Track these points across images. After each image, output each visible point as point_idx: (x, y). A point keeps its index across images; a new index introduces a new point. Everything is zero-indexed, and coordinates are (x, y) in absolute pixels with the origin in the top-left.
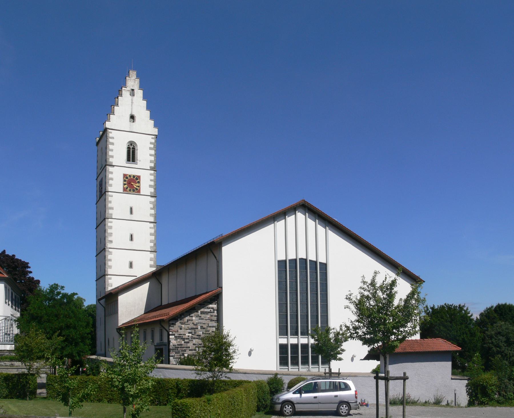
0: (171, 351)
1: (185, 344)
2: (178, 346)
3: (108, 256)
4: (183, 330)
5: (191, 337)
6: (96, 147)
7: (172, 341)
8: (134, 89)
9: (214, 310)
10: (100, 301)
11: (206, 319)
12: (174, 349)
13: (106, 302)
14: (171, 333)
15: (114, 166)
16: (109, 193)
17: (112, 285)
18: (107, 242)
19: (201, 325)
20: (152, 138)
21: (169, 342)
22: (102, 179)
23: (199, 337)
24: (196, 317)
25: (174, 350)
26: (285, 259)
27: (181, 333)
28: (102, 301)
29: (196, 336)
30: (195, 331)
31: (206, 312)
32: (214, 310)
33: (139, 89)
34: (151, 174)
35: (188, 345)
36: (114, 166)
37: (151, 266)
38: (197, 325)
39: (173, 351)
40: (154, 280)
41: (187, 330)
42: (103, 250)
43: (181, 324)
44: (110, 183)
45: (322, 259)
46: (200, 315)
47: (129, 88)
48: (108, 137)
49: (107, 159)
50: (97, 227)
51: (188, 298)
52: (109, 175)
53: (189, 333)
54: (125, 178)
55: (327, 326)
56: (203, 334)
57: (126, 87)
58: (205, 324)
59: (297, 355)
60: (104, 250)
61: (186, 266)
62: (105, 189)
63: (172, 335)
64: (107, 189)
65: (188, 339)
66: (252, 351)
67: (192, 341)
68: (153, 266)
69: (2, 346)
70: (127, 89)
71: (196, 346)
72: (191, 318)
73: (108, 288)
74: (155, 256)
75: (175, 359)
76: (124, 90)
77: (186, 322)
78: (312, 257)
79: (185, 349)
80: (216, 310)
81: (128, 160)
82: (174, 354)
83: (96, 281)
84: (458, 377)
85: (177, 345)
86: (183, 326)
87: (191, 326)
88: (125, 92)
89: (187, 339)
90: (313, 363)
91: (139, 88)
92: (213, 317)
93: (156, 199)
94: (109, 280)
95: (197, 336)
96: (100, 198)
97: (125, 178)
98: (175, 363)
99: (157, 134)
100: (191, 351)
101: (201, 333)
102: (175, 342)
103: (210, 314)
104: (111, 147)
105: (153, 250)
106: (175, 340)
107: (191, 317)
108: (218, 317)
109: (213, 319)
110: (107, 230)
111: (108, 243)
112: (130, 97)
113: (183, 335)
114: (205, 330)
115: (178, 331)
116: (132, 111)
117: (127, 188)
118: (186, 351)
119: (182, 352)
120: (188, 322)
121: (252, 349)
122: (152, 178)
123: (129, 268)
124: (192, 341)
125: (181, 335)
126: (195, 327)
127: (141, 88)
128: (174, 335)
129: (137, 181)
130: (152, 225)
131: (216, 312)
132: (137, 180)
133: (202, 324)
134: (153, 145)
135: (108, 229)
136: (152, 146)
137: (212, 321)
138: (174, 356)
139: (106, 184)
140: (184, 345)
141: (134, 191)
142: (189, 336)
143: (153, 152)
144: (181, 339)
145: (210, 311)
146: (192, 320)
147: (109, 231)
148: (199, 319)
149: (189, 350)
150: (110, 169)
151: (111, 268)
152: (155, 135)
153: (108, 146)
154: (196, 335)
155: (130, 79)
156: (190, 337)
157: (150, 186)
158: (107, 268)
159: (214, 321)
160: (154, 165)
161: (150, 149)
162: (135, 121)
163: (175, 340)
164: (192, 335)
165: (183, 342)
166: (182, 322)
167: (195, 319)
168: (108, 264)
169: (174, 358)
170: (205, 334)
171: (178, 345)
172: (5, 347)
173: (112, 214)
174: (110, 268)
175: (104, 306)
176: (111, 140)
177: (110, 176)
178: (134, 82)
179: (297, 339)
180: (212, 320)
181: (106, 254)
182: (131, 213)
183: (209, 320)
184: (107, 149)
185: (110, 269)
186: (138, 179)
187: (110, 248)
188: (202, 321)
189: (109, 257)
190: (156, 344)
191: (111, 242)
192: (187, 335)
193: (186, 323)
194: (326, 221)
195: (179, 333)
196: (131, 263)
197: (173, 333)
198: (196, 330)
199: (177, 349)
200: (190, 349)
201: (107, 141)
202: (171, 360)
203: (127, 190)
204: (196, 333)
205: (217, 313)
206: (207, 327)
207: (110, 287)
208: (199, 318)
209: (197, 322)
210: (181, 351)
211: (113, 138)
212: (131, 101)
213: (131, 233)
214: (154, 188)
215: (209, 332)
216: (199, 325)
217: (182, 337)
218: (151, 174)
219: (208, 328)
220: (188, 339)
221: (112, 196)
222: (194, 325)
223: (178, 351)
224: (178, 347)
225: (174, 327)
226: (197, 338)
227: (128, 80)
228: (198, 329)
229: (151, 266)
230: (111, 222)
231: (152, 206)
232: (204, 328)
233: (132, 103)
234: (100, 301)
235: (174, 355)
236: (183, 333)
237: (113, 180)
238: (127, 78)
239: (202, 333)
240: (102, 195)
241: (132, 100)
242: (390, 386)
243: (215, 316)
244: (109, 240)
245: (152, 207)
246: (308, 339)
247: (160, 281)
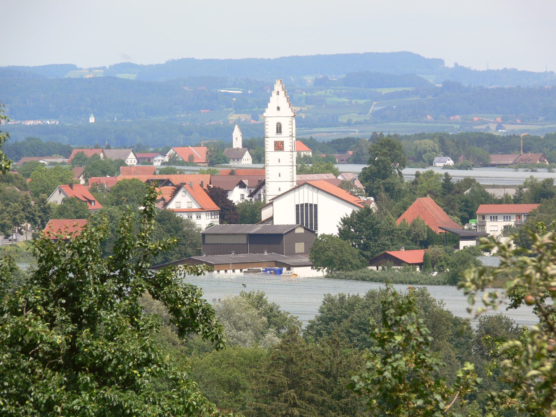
81: (277, 132)
88: (274, 94)
150: (266, 139)
182: (279, 162)
211: (268, 122)
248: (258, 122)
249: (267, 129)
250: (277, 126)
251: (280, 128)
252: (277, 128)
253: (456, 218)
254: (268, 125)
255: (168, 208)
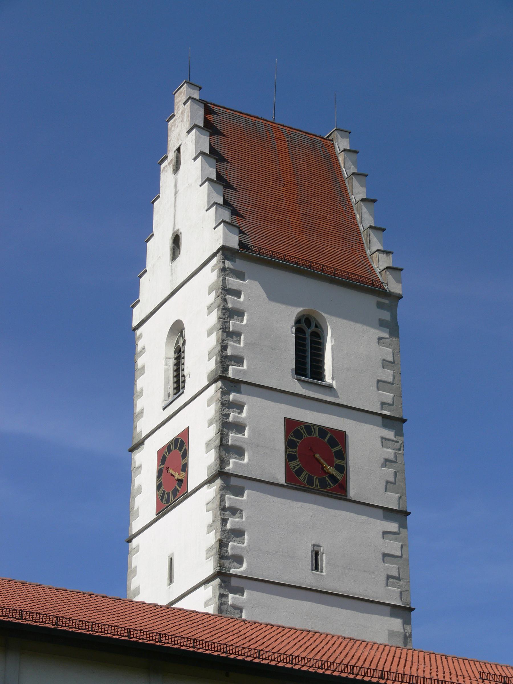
10: (399, 532)
54: (291, 433)
55: (239, 340)
84: (302, 335)
97: (291, 433)
117: (299, 472)
129: (334, 450)
132: (325, 438)
182: (316, 566)
186: (338, 445)
203: (302, 478)
234: (399, 532)
242: (350, 476)
246: (233, 476)
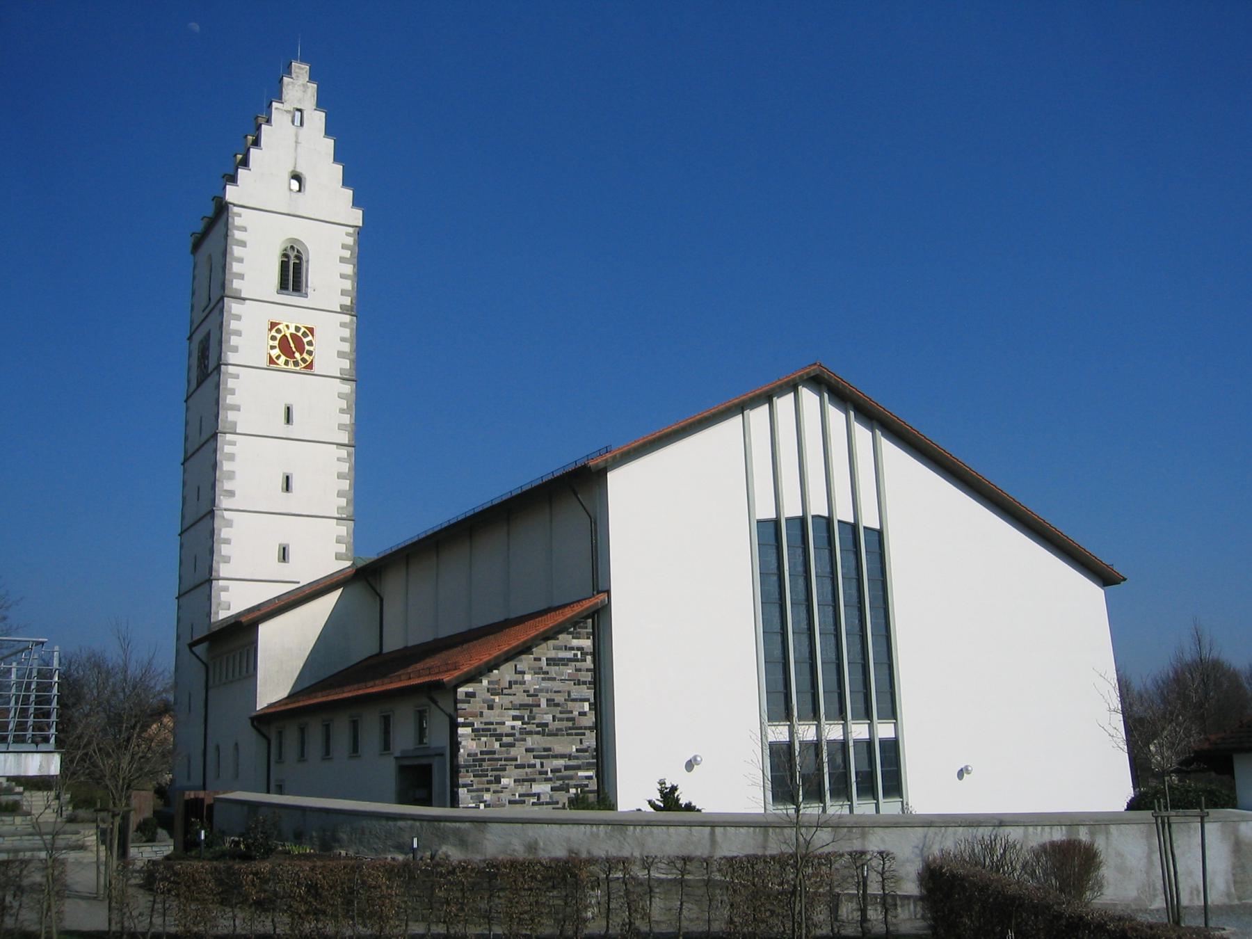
0: (462, 770)
1: (503, 749)
2: (485, 756)
3: (220, 530)
4: (496, 711)
5: (520, 729)
6: (192, 256)
7: (464, 743)
8: (303, 108)
9: (584, 654)
10: (194, 649)
11: (563, 678)
12: (469, 766)
13: (209, 650)
14: (461, 720)
15: (244, 299)
16: (230, 367)
17: (230, 606)
18: (220, 495)
19: (549, 696)
20: (348, 234)
21: (455, 745)
22: (209, 334)
23: (544, 730)
24: (535, 673)
25: (470, 767)
26: (774, 517)
27: (492, 720)
28: (200, 649)
29: (535, 726)
30: (531, 712)
31: (563, 659)
32: (584, 654)
33: (315, 110)
34: (343, 325)
35: (512, 753)
36: (244, 299)
37: (339, 557)
38: (537, 695)
39: (467, 771)
40: (358, 589)
41: (509, 711)
42: (205, 516)
43: (491, 695)
44: (232, 343)
45: (869, 520)
46: (545, 668)
47: (288, 106)
48: (230, 226)
49: (226, 282)
50: (186, 460)
51: (443, 639)
52: (232, 321)
53: (515, 718)
56: (554, 720)
57: (282, 103)
58: (559, 692)
59: (895, 768)
60: (209, 517)
61: (438, 556)
62: (220, 358)
63: (465, 725)
64: (223, 358)
65: (512, 735)
66: (698, 764)
67: (524, 740)
68: (344, 557)
69: (5, 761)
70: (285, 108)
71: (534, 753)
72: (521, 676)
73: (217, 613)
74: (351, 531)
75: (474, 794)
76: (276, 108)
77: (506, 688)
78: (844, 513)
79: (503, 763)
80: (591, 654)
81: (283, 286)
82: (472, 779)
83: (176, 598)
85: (479, 754)
86: (497, 699)
87: (522, 698)
88: (279, 113)
89: (508, 735)
90: (860, 793)
91: (315, 107)
92: (582, 673)
93: (354, 387)
94: (222, 593)
95: (537, 727)
96: (199, 385)
98: (474, 805)
99: (361, 225)
100: (520, 770)
101: (548, 718)
102: (475, 746)
103: (573, 664)
104: (237, 251)
105: (344, 516)
106: (472, 740)
107: (518, 675)
108: (595, 674)
109: (582, 679)
110: (221, 462)
111: (222, 497)
112: (292, 129)
113: (497, 723)
114: (560, 708)
115: (482, 713)
116: (296, 164)
118: (505, 770)
119: (494, 772)
120: (510, 687)
121: (699, 759)
122: (347, 333)
123: (279, 561)
124: (524, 740)
125: (492, 724)
126: (530, 700)
127: (320, 105)
128: (472, 725)
130: (343, 453)
131: (589, 658)
133: (551, 692)
134: (350, 252)
135: (224, 462)
136: (347, 254)
137: (579, 684)
138: (472, 785)
139: (221, 346)
140: (501, 753)
141: (298, 366)
142: (513, 728)
143: (349, 269)
144: (491, 735)
145: (572, 656)
146: (523, 683)
147: (226, 466)
148: (543, 679)
149: (513, 767)
150: (233, 307)
151: (229, 562)
152: (356, 227)
153: (231, 248)
154: (533, 724)
155: (292, 83)
156: (517, 729)
157: (341, 354)
158: (218, 563)
159: (584, 683)
160: (351, 302)
161: (342, 260)
162: (302, 188)
163: (475, 740)
164: (523, 724)
165: (497, 745)
166: (495, 689)
167: (530, 679)
168: (221, 552)
169: (468, 791)
170: (561, 720)
171: (482, 753)
172: (19, 764)
173: (235, 424)
174: (225, 562)
175: (204, 659)
176: (238, 235)
177: (234, 325)
178: (304, 92)
179: (893, 725)
180: (579, 680)
181: (215, 526)
182: (288, 420)
183: (573, 683)
184: (228, 256)
185: (226, 564)
186: (308, 336)
187: (225, 510)
188: (550, 685)
189: (224, 533)
190: (397, 754)
191: (231, 494)
192: (509, 723)
193: (505, 691)
194: (875, 422)
195: (484, 720)
196: (284, 549)
197: (467, 721)
198: (534, 709)
199: (480, 766)
200: (519, 762)
201: (227, 236)
202: (460, 795)
204: (534, 719)
205: (594, 662)
206: (565, 700)
207: (223, 611)
208: (543, 676)
209: (537, 687)
210: (492, 770)
211: (244, 229)
212: (294, 139)
213: (285, 471)
214: (350, 360)
215: (570, 715)
216: (543, 697)
217: (495, 730)
218: (343, 325)
219: (570, 704)
220: (512, 735)
221: (237, 377)
222: (528, 696)
223: (481, 771)
224: (484, 760)
225: (469, 703)
226: (538, 733)
227: (288, 84)
228: (539, 706)
229: (339, 557)
230: (233, 443)
231: (344, 404)
232: (557, 705)
233: (297, 142)
235: (472, 781)
236: (499, 720)
237: (240, 336)
238: (286, 79)
239: (551, 718)
240: (208, 375)
241: (297, 136)
243: (588, 670)
244: (225, 488)
245: (345, 407)
247: (378, 591)
248: (308, 363)
249: (241, 260)
250: (285, 255)
251: (298, 268)
252: (284, 266)
253: (866, 843)
254: (243, 244)
255: (258, 709)
